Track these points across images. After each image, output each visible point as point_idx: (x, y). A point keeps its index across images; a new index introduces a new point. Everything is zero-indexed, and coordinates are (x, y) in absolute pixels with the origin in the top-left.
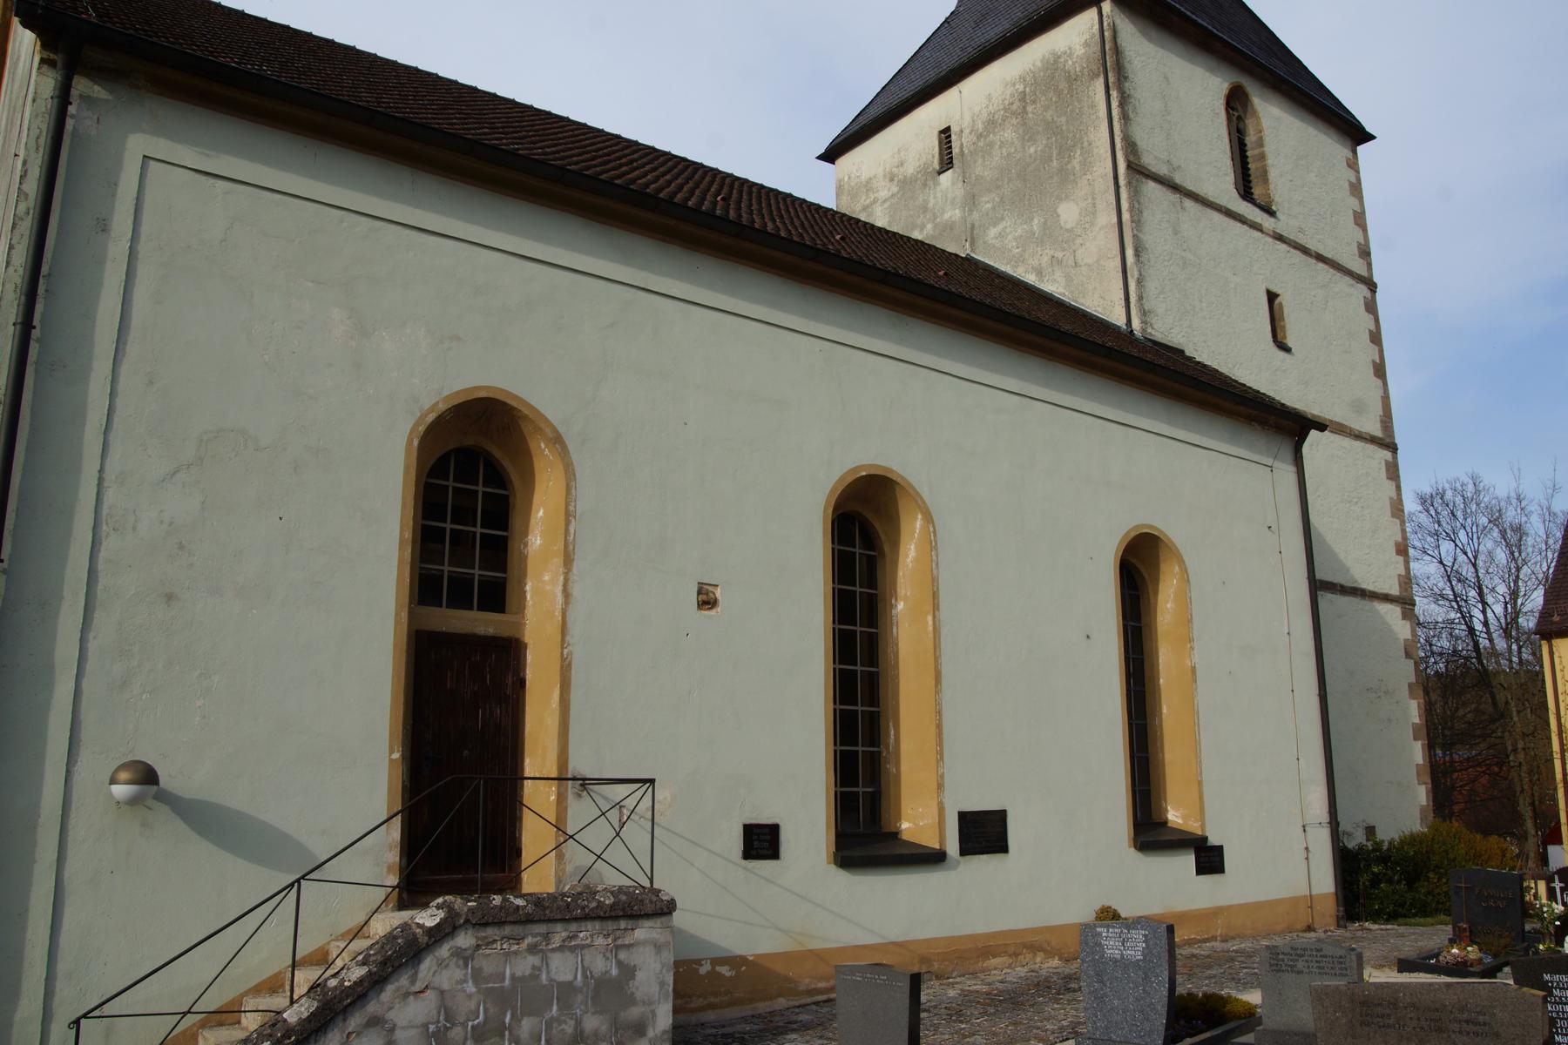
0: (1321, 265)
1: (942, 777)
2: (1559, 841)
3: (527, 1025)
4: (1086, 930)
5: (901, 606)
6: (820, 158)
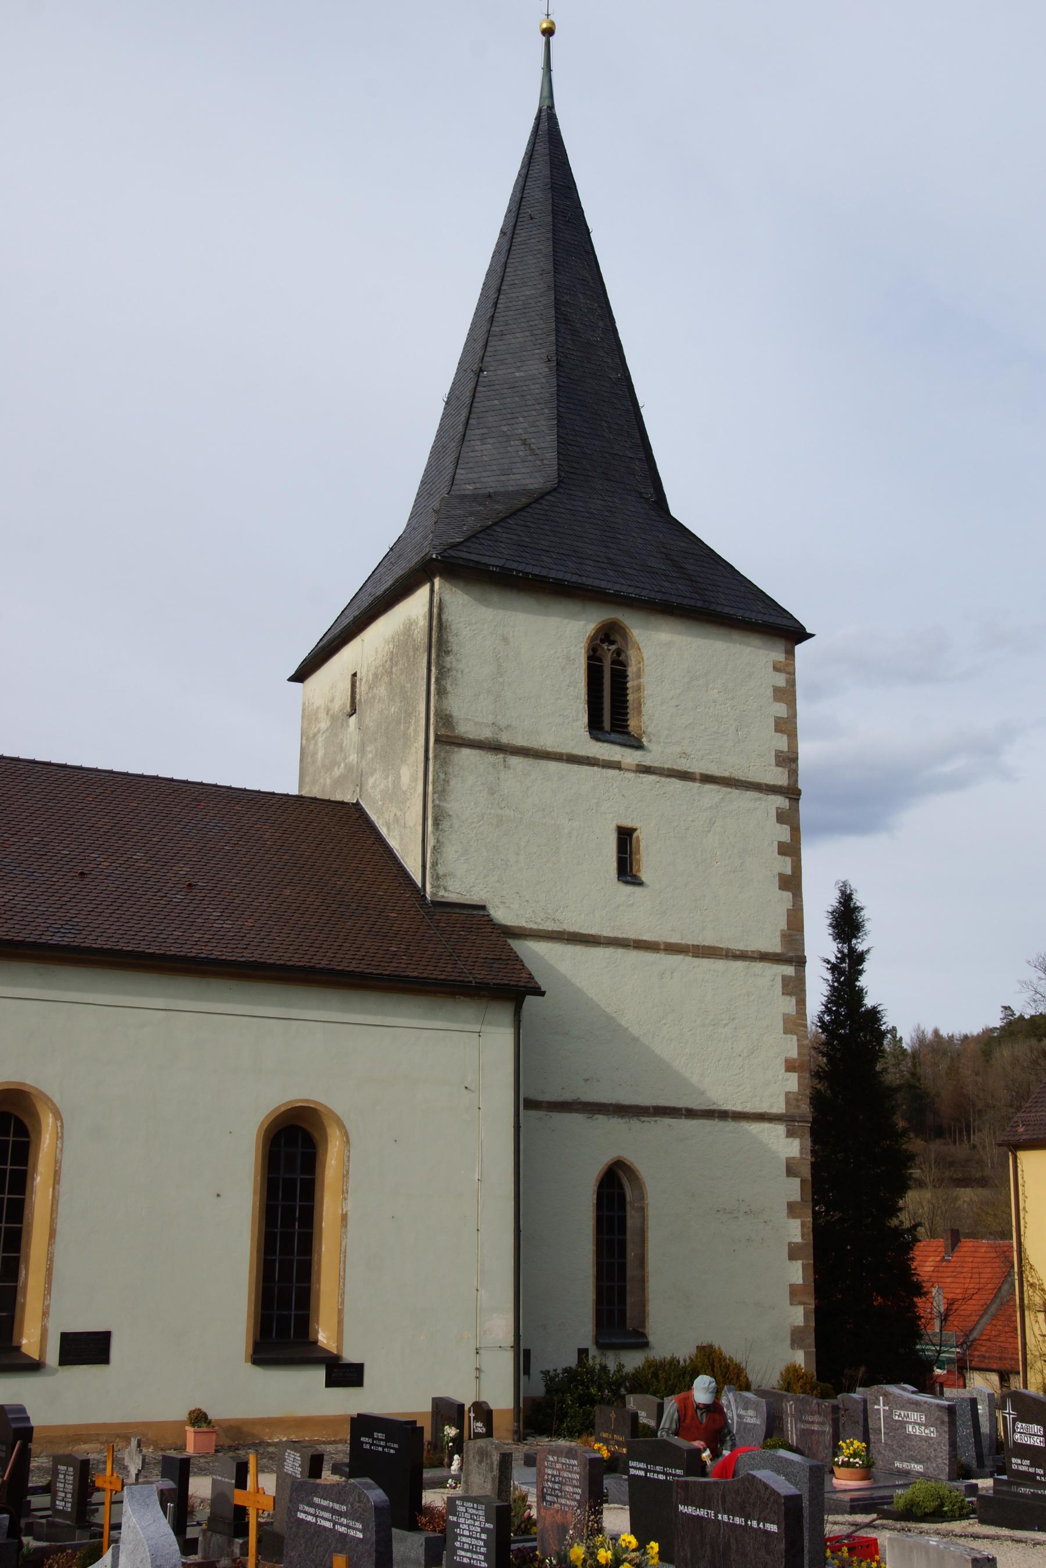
0: (708, 787)
1: (48, 1306)
5: (38, 1179)
6: (290, 680)
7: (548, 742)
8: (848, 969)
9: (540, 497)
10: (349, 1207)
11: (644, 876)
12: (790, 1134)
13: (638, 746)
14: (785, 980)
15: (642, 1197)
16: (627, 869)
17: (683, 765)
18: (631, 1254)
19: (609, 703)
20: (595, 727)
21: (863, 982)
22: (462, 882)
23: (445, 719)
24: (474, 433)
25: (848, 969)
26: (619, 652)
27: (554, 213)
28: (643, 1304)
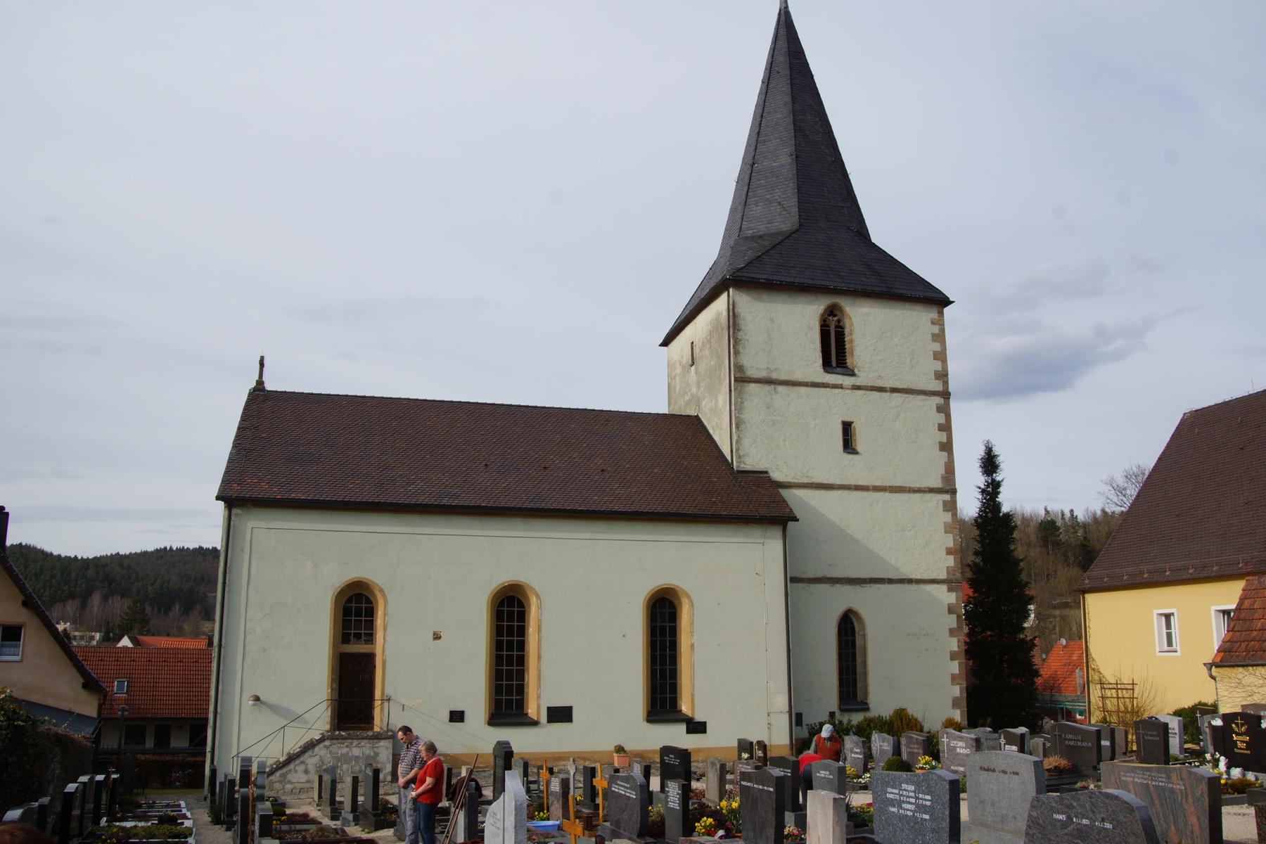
0: (895, 395)
2: (688, 732)
3: (345, 767)
4: (610, 753)
6: (662, 345)
7: (799, 376)
8: (991, 492)
9: (790, 235)
10: (695, 639)
11: (859, 449)
12: (950, 590)
13: (853, 374)
14: (945, 503)
15: (864, 629)
16: (849, 445)
17: (879, 383)
18: (859, 660)
19: (835, 351)
20: (827, 365)
21: (1000, 498)
22: (753, 458)
23: (740, 368)
24: (751, 200)
25: (991, 492)
26: (839, 321)
27: (791, 69)
28: (866, 687)
